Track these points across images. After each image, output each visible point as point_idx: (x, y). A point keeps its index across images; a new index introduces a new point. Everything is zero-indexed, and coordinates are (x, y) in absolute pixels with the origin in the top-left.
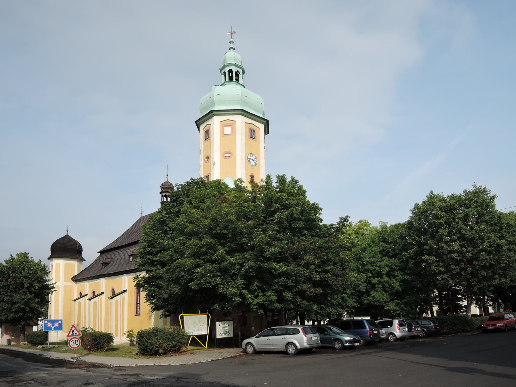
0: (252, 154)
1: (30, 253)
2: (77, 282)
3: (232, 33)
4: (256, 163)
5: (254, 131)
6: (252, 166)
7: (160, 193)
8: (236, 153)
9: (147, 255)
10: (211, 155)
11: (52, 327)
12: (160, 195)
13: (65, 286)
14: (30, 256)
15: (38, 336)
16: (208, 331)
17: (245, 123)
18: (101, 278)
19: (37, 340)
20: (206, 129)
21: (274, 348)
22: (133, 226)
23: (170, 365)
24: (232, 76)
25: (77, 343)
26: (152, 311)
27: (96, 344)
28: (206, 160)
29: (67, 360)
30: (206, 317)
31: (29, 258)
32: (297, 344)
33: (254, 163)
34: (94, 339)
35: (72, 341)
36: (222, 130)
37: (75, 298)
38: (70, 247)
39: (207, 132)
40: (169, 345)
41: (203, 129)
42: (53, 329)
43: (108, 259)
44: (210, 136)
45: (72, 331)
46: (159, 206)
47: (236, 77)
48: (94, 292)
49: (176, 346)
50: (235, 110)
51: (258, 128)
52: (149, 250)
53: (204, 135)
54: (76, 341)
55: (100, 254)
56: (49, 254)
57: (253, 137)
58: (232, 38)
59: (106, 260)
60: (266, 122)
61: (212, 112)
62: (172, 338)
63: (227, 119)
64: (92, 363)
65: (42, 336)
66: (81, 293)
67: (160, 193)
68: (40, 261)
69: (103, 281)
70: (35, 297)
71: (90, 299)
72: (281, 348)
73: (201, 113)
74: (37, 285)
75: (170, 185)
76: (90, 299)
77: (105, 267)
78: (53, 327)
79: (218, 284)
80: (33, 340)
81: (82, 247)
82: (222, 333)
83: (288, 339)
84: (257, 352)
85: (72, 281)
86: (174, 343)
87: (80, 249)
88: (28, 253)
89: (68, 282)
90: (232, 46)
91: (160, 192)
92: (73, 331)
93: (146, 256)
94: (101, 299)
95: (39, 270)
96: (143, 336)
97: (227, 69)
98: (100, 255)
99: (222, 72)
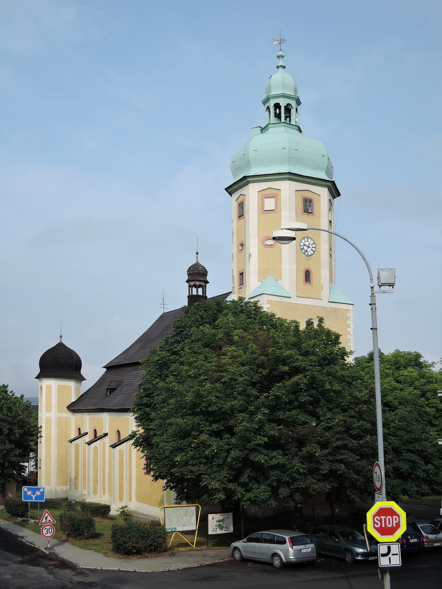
0: (308, 238)
1: (9, 386)
2: (74, 412)
3: (281, 41)
5: (311, 201)
6: (308, 256)
7: (187, 281)
9: (145, 406)
10: (245, 243)
11: (32, 495)
13: (59, 419)
14: (9, 389)
15: (17, 506)
16: (197, 526)
18: (104, 412)
19: (16, 510)
21: (260, 557)
22: (151, 328)
23: (135, 571)
24: (280, 112)
25: (51, 532)
26: (153, 480)
27: (75, 531)
28: (240, 248)
29: (41, 550)
30: (194, 508)
31: (8, 392)
32: (283, 557)
33: (311, 251)
34: (72, 525)
35: (45, 529)
37: (73, 437)
38: (64, 362)
39: (241, 206)
40: (143, 544)
41: (236, 200)
42: (34, 499)
43: (114, 383)
44: (244, 214)
45: (45, 518)
46: (185, 302)
48: (95, 430)
49: (152, 546)
50: (279, 174)
52: (147, 401)
53: (238, 209)
54: (50, 529)
55: (106, 369)
56: (37, 371)
57: (310, 211)
58: (280, 50)
59: (111, 385)
60: (330, 184)
61: (246, 179)
62: (147, 536)
63: (268, 187)
64: (63, 559)
65: (22, 506)
66: (79, 429)
67: (187, 281)
68: (22, 396)
69: (106, 417)
70: (16, 447)
71: (89, 443)
72: (267, 558)
73: (234, 176)
74: (17, 431)
75: (200, 269)
76: (89, 443)
77: (109, 395)
79: (202, 474)
80: (12, 510)
81: (81, 361)
82: (217, 529)
83: (274, 548)
84: (244, 560)
85: (68, 411)
86: (149, 543)
87: (78, 364)
88: (7, 386)
89: (62, 412)
90: (281, 63)
91: (186, 280)
92: (46, 518)
93: (143, 408)
94: (104, 443)
95: (20, 410)
96: (116, 531)
97: (272, 103)
98: (106, 372)
99: (266, 106)
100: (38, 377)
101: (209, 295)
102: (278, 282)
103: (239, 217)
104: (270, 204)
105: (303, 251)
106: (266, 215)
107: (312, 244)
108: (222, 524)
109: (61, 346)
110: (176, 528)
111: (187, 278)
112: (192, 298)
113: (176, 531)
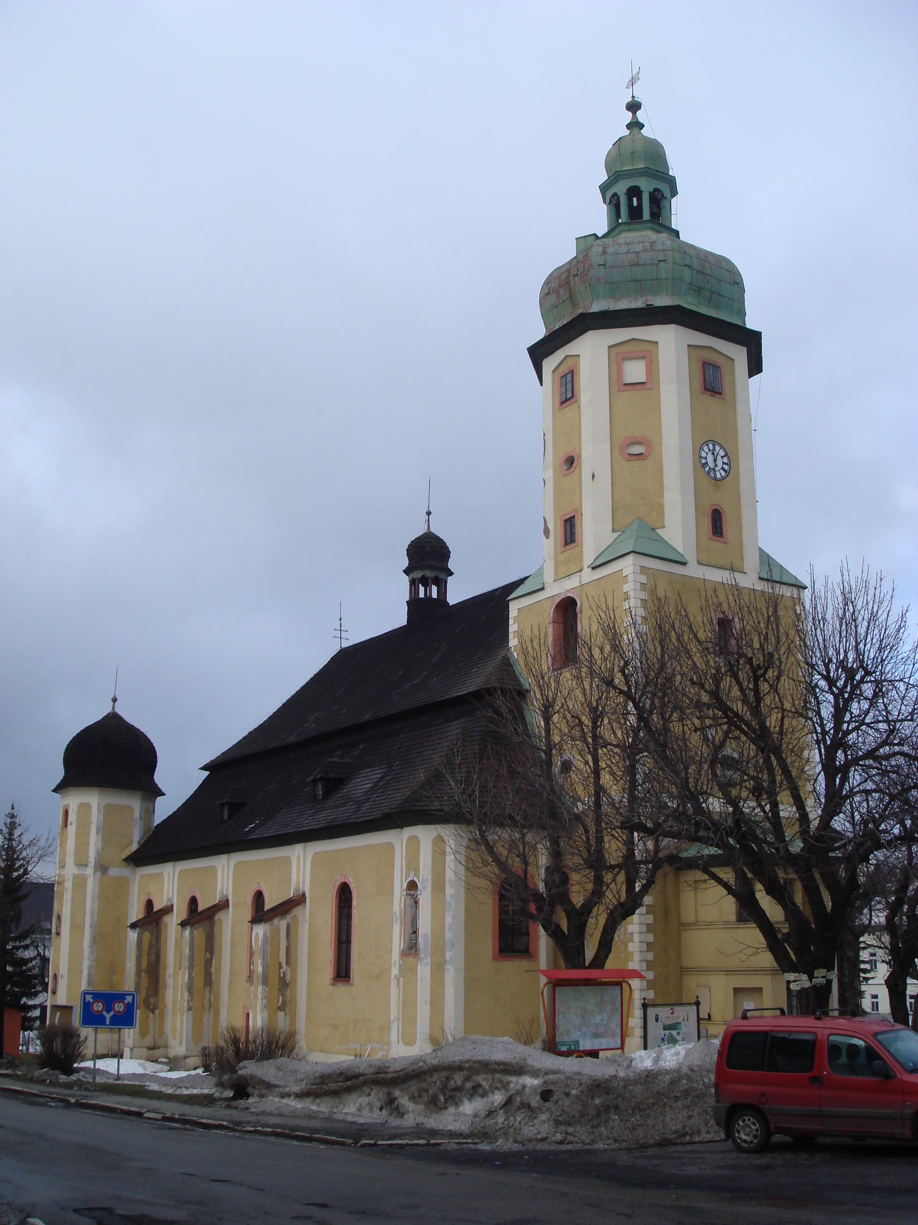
4: (725, 471)
7: (407, 572)
8: (660, 443)
11: (105, 1013)
12: (406, 579)
17: (688, 345)
20: (563, 369)
33: (721, 471)
36: (615, 371)
42: (108, 1022)
47: (651, 208)
51: (729, 358)
56: (59, 773)
67: (407, 572)
77: (230, 816)
78: (108, 1016)
100: (59, 789)
101: (453, 598)
102: (656, 532)
103: (562, 403)
104: (635, 371)
105: (707, 469)
106: (627, 395)
107: (722, 457)
108: (676, 1036)
109: (527, 349)
110: (578, 1042)
111: (405, 563)
112: (414, 604)
113: (577, 1049)
